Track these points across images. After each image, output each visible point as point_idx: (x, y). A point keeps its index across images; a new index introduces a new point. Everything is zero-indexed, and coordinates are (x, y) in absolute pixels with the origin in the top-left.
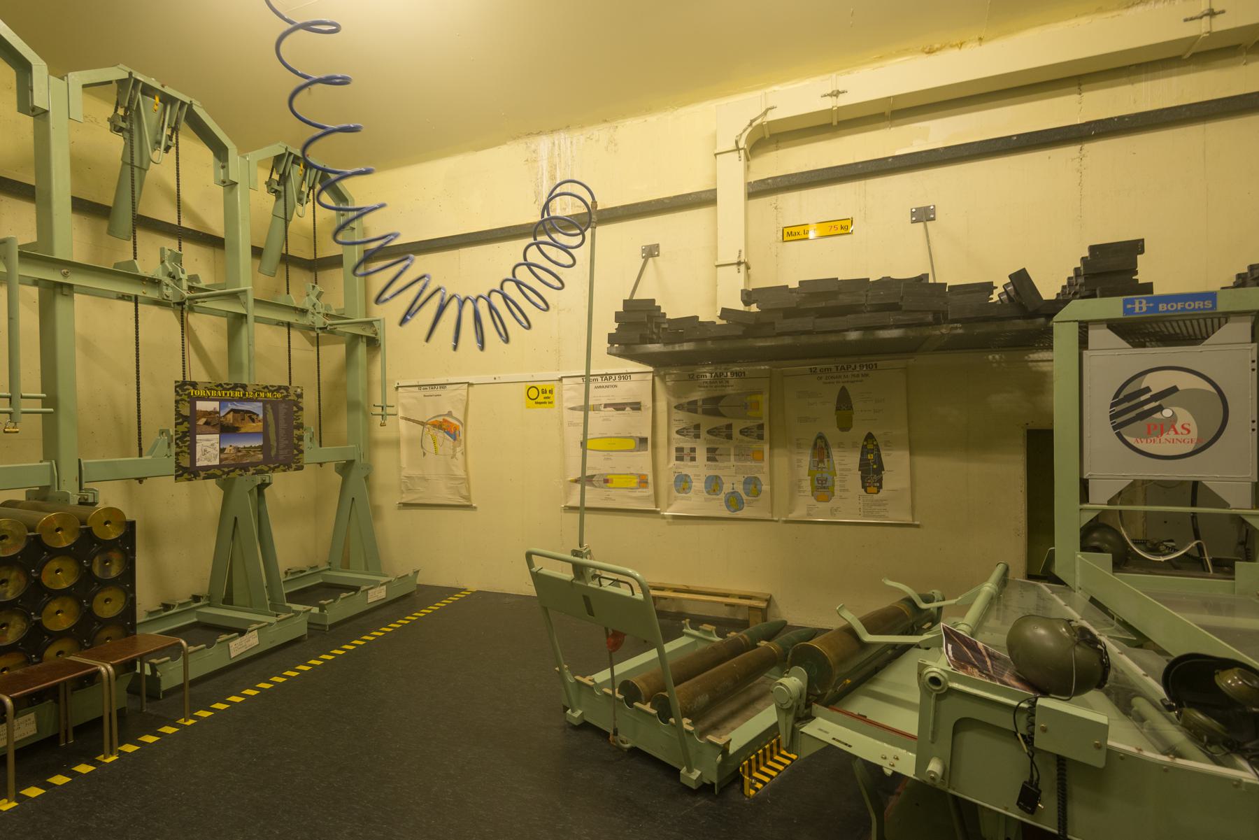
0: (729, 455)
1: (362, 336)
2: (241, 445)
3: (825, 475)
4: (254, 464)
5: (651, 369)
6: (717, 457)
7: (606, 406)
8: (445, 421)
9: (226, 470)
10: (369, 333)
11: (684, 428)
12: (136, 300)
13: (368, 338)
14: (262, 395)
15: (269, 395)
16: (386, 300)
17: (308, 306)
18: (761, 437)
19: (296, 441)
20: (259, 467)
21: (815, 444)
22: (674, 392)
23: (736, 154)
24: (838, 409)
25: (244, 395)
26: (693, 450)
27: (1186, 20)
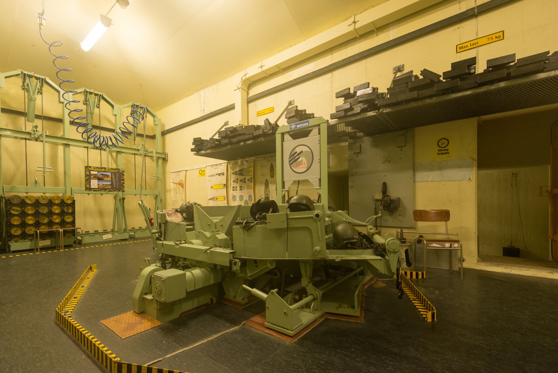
0: (245, 188)
1: (160, 157)
2: (104, 183)
3: (268, 193)
4: (108, 189)
5: (227, 161)
6: (242, 189)
7: (217, 174)
8: (181, 182)
9: (100, 189)
10: (163, 156)
11: (235, 180)
12: (87, 148)
13: (162, 158)
14: (111, 171)
15: (113, 171)
16: (90, 138)
17: (140, 148)
18: (251, 182)
19: (122, 184)
20: (110, 190)
21: (265, 183)
22: (233, 169)
23: (239, 90)
24: (270, 171)
25: (105, 170)
26: (236, 187)
27: (349, 26)
